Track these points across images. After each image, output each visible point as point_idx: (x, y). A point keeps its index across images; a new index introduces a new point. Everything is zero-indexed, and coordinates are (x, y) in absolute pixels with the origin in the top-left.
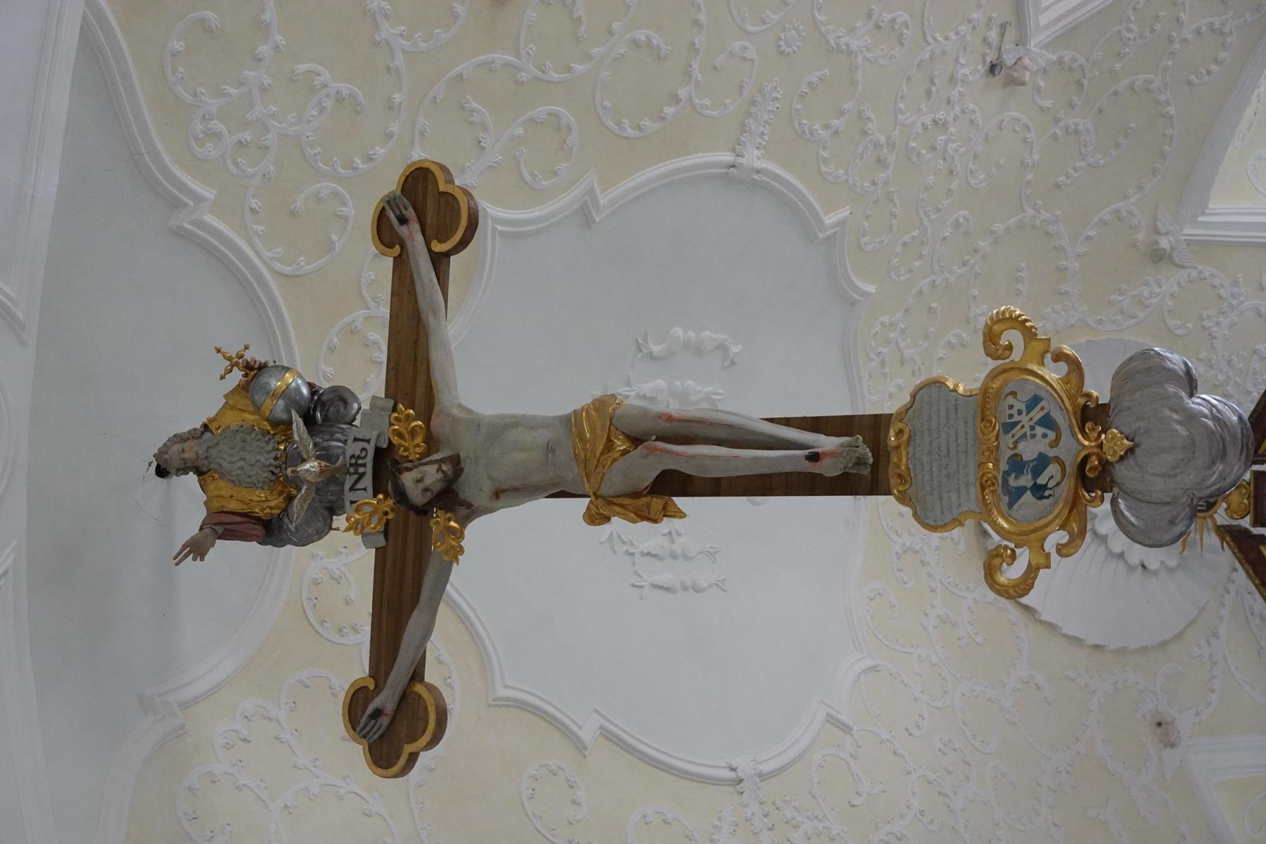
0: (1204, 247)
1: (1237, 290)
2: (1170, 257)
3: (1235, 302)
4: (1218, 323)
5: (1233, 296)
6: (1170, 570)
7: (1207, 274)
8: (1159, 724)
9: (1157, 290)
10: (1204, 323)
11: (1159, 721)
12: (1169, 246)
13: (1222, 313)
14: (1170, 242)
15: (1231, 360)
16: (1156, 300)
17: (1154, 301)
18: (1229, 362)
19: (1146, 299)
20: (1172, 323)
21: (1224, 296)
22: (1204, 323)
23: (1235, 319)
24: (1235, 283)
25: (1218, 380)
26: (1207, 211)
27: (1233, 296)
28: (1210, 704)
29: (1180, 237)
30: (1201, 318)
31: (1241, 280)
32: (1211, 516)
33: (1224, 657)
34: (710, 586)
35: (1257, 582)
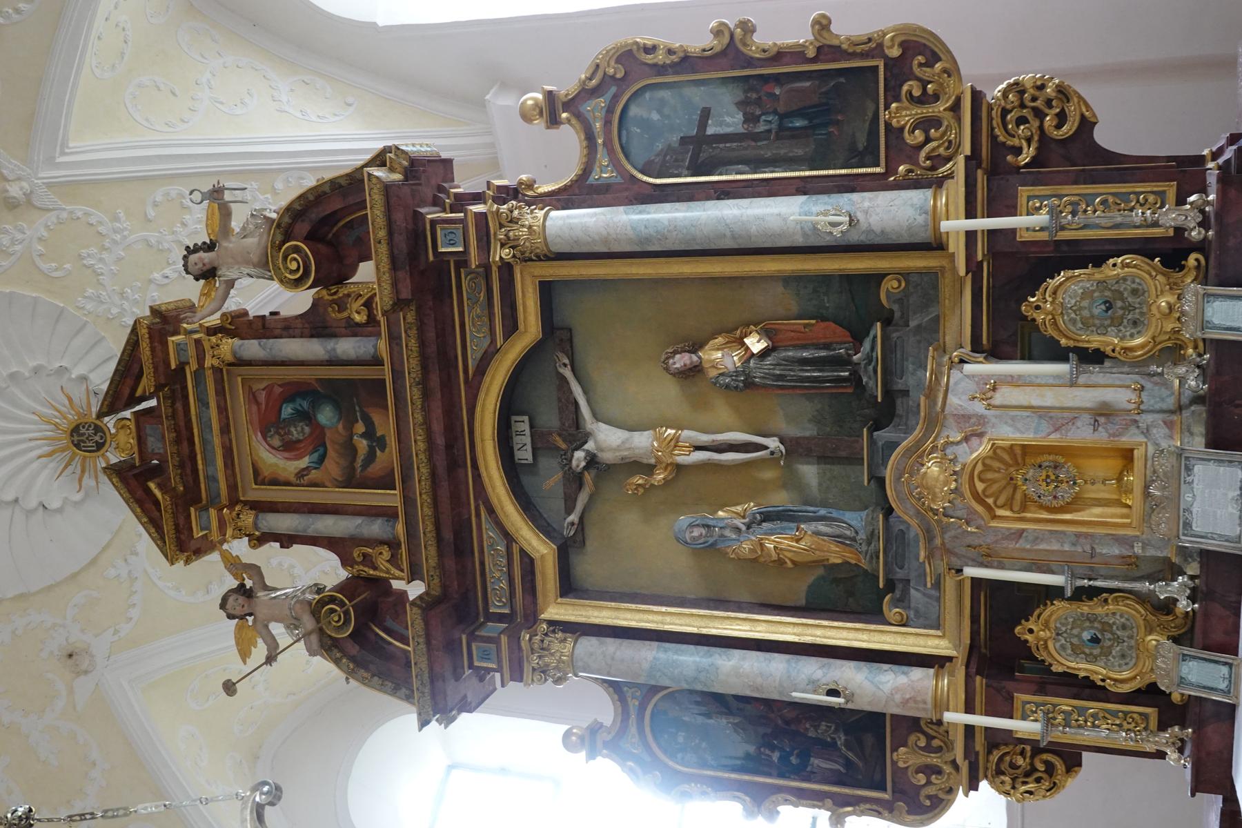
0: (68, 189)
1: (118, 225)
2: (29, 203)
3: (118, 237)
4: (101, 260)
5: (115, 231)
6: (76, 504)
7: (80, 214)
8: (70, 656)
9: (19, 236)
10: (85, 262)
11: (69, 652)
12: (21, 193)
13: (103, 248)
14: (21, 189)
15: (124, 293)
16: (20, 246)
17: (18, 248)
18: (122, 295)
19: (8, 247)
20: (44, 266)
21: (104, 232)
22: (85, 262)
23: (122, 254)
24: (116, 218)
25: (112, 314)
26: (67, 151)
27: (115, 231)
28: (131, 619)
29: (36, 181)
30: (81, 258)
31: (122, 214)
32: (103, 455)
33: (145, 571)
34: (190, 274)
35: (145, 520)
